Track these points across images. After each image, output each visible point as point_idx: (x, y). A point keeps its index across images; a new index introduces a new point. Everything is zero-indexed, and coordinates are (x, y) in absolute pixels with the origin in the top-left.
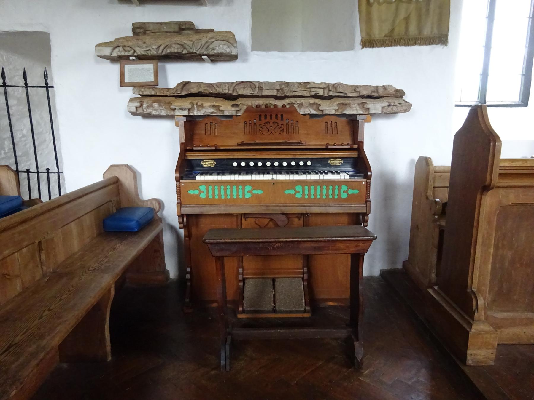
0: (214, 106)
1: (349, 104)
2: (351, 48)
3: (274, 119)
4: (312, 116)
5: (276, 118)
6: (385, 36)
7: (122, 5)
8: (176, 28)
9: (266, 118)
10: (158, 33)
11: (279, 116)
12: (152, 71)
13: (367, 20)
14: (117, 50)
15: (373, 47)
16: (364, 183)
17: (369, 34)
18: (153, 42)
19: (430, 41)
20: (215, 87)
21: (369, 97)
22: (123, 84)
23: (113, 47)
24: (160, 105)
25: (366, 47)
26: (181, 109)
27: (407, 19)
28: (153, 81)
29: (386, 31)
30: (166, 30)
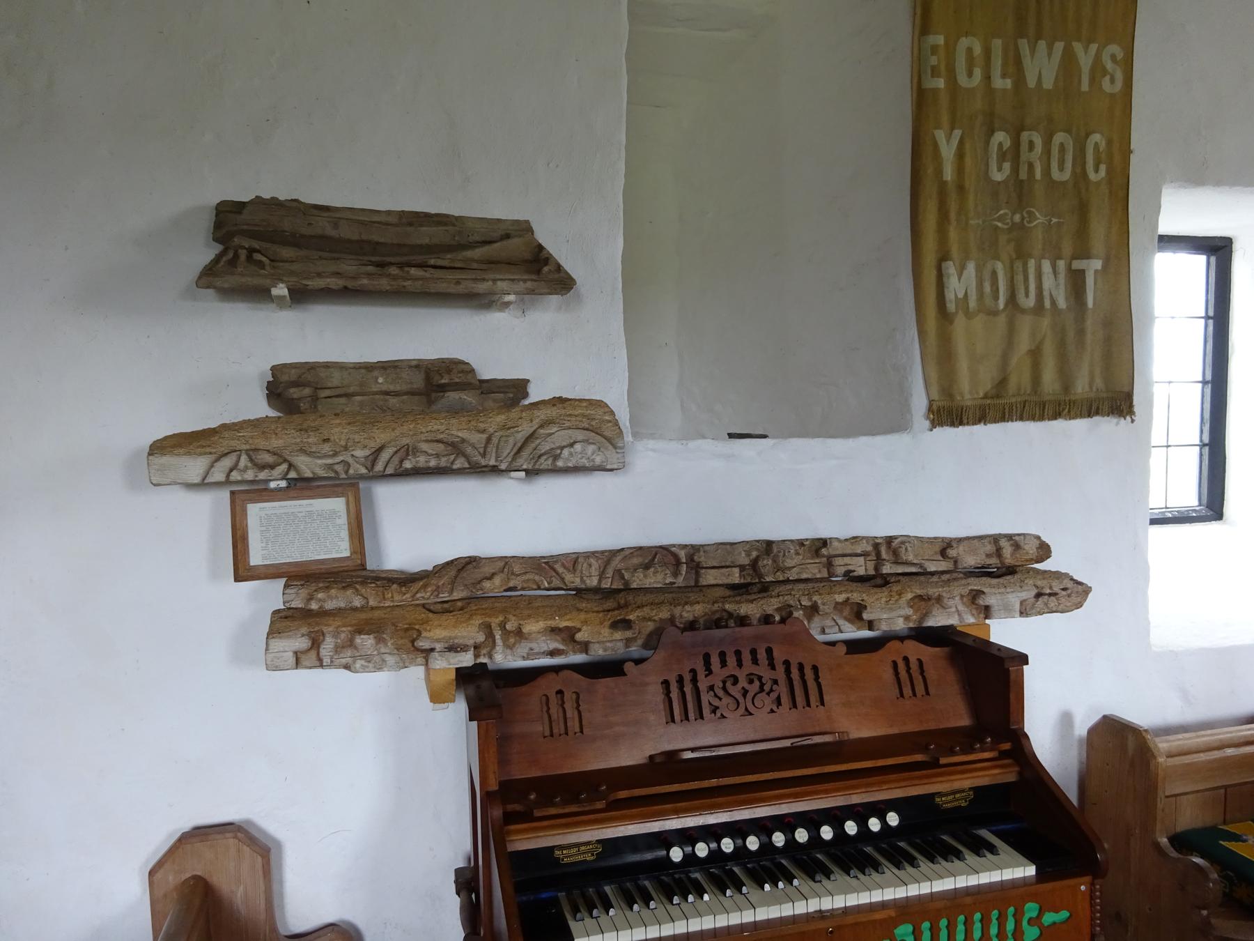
0: (554, 630)
1: (939, 599)
2: (897, 424)
3: (748, 667)
4: (854, 647)
5: (755, 661)
6: (985, 397)
7: (227, 306)
8: (418, 381)
9: (724, 663)
10: (358, 398)
11: (762, 655)
12: (343, 520)
13: (942, 358)
14: (227, 462)
15: (961, 423)
16: (1083, 888)
17: (948, 389)
18: (357, 438)
19: (1090, 409)
20: (560, 570)
21: (983, 572)
22: (243, 572)
23: (213, 457)
24: (380, 640)
25: (941, 424)
26: (453, 648)
27: (1035, 354)
28: (347, 554)
29: (986, 385)
30: (384, 388)
